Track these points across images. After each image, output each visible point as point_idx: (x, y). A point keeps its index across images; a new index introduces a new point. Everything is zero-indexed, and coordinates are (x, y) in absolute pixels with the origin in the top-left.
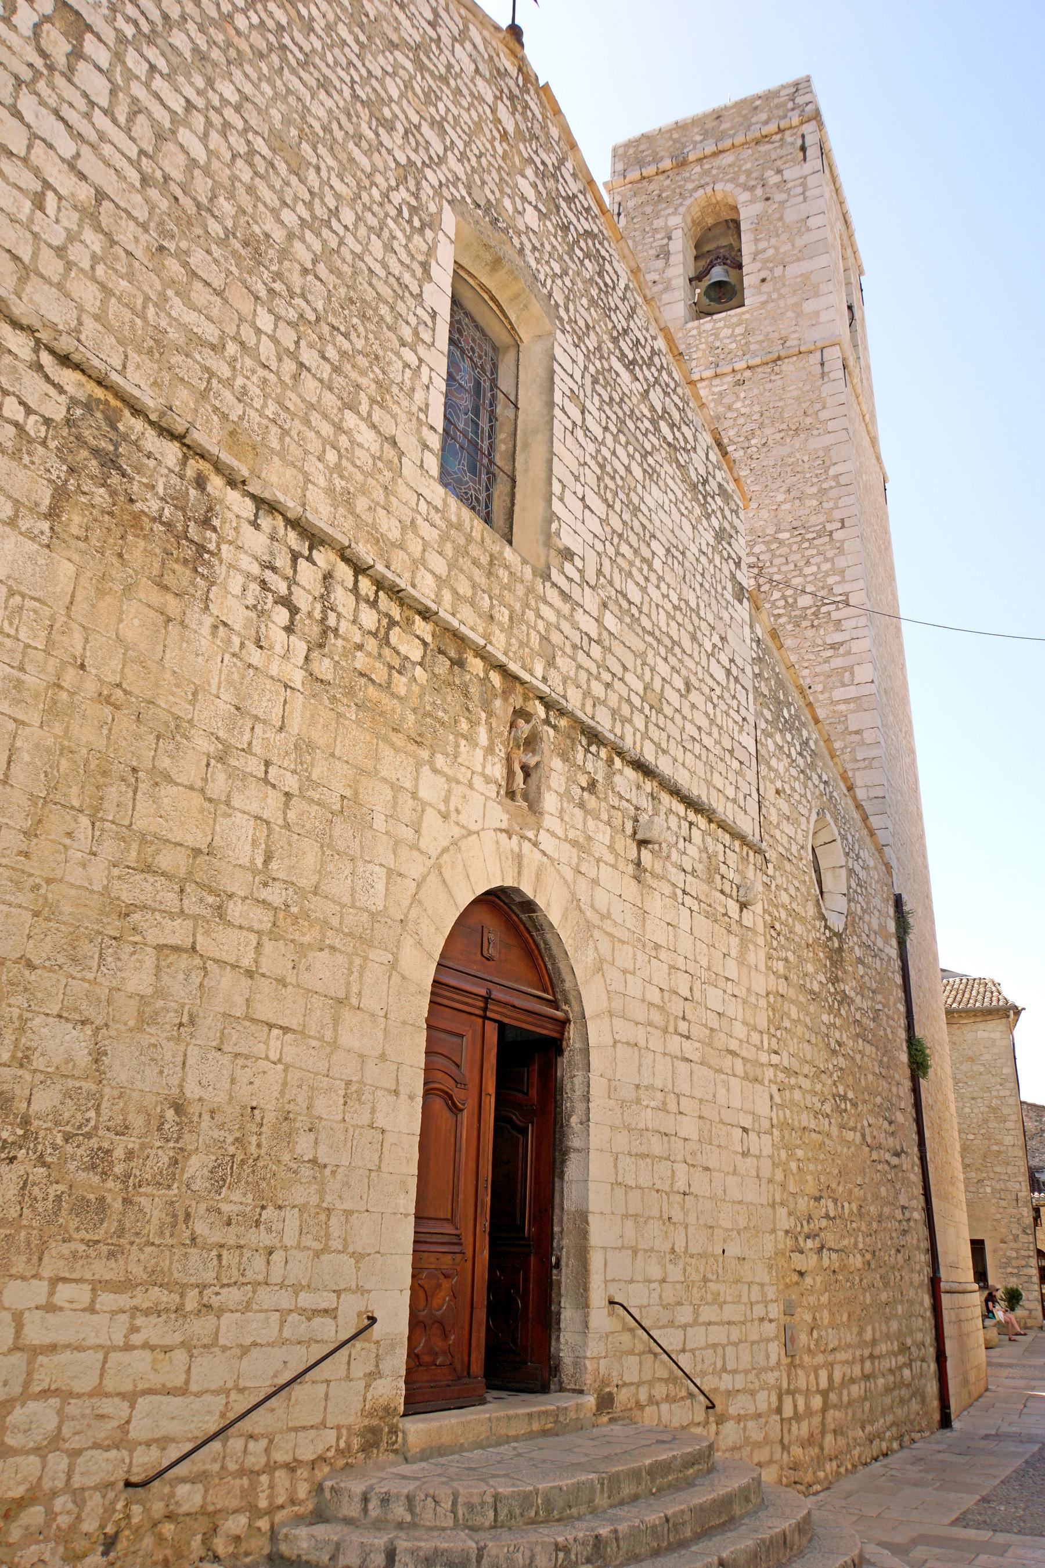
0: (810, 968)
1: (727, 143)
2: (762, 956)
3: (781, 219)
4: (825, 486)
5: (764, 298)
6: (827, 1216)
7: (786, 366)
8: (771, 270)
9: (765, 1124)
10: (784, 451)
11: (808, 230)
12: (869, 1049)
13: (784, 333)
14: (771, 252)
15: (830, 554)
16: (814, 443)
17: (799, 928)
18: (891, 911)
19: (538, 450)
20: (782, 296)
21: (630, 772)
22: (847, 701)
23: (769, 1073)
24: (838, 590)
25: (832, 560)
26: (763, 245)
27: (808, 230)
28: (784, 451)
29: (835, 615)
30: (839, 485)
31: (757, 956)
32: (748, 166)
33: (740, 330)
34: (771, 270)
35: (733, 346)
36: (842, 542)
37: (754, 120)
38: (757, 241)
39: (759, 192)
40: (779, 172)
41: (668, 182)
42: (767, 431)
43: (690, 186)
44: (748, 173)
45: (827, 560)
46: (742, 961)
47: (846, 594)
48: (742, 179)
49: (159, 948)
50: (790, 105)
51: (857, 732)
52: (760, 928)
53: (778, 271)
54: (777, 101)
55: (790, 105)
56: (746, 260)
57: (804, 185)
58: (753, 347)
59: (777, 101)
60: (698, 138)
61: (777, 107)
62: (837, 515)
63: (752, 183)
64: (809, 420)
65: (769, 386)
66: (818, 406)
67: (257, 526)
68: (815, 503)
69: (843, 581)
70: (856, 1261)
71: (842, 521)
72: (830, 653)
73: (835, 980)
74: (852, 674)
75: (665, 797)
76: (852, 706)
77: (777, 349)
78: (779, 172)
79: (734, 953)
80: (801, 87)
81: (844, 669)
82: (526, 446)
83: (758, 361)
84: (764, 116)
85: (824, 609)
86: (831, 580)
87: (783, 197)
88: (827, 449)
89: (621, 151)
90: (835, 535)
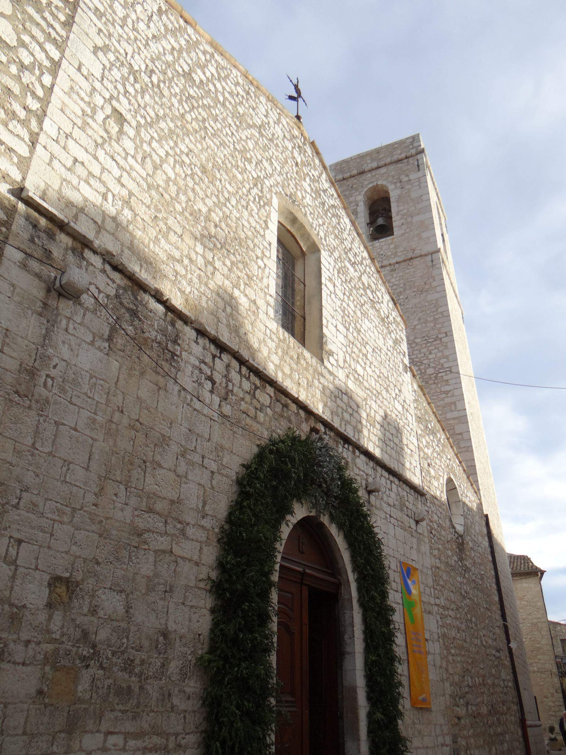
0: (449, 553)
1: (383, 163)
2: (428, 548)
3: (409, 196)
4: (437, 317)
5: (403, 232)
6: (468, 686)
7: (416, 262)
8: (406, 219)
9: (436, 636)
10: (416, 301)
11: (422, 201)
12: (480, 594)
14: (405, 211)
15: (441, 349)
16: (429, 298)
17: (443, 533)
18: (484, 523)
20: (411, 230)
21: (363, 457)
22: (454, 419)
23: (436, 608)
24: (446, 365)
25: (442, 352)
26: (401, 208)
27: (422, 201)
28: (416, 301)
29: (445, 378)
30: (443, 316)
31: (425, 548)
32: (393, 173)
33: (392, 246)
34: (406, 219)
35: (390, 253)
36: (447, 343)
37: (395, 153)
38: (398, 206)
39: (398, 185)
40: (407, 176)
41: (355, 181)
42: (408, 292)
43: (366, 183)
45: (439, 351)
46: (419, 551)
47: (450, 367)
48: (390, 179)
49: (156, 551)
50: (411, 147)
51: (459, 434)
52: (426, 534)
53: (409, 219)
54: (405, 145)
55: (411, 147)
58: (399, 254)
59: (405, 145)
60: (369, 161)
61: (406, 147)
62: (443, 330)
63: (395, 181)
64: (427, 287)
65: (407, 271)
66: (431, 280)
67: (197, 343)
68: (432, 325)
69: (448, 361)
70: (484, 710)
72: (444, 396)
73: (461, 559)
74: (455, 405)
75: (379, 469)
76: (456, 421)
77: (410, 255)
78: (407, 176)
79: (415, 547)
80: (415, 139)
81: (452, 403)
83: (401, 259)
84: (399, 152)
85: (440, 375)
88: (437, 300)
89: (333, 168)
90: (443, 340)
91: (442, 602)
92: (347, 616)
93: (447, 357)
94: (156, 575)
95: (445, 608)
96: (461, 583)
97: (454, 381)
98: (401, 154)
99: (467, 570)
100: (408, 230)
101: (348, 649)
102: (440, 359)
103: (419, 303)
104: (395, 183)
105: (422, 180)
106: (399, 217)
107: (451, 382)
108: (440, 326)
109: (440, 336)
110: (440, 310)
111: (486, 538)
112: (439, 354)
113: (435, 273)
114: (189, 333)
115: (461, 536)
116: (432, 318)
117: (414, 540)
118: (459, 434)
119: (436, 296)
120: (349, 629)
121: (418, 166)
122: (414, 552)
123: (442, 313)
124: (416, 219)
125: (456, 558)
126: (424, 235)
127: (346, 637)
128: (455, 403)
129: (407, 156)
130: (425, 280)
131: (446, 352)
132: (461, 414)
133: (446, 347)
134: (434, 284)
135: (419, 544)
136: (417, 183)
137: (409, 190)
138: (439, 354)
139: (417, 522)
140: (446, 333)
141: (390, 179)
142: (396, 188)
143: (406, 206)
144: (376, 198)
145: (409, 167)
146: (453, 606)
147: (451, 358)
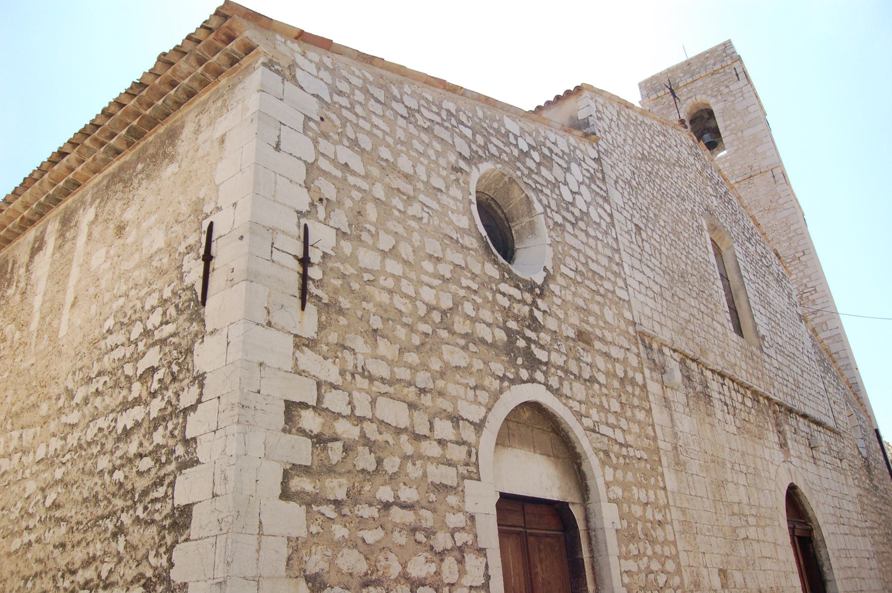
13: (750, 164)
14: (733, 125)
17: (856, 462)
19: (742, 297)
21: (801, 420)
24: (809, 285)
26: (728, 122)
29: (811, 298)
37: (708, 63)
38: (725, 121)
39: (719, 97)
44: (712, 89)
45: (800, 271)
47: (814, 287)
48: (709, 92)
51: (836, 353)
55: (724, 55)
56: (721, 131)
57: (741, 91)
60: (681, 75)
61: (718, 56)
62: (800, 249)
64: (774, 205)
65: (749, 190)
69: (811, 280)
71: (803, 251)
72: (813, 316)
73: (871, 480)
74: (826, 325)
76: (830, 341)
78: (727, 87)
81: (822, 323)
82: (737, 296)
83: (740, 179)
84: (712, 61)
85: (804, 295)
86: (805, 281)
87: (732, 99)
89: (643, 85)
91: (868, 524)
92: (822, 553)
93: (809, 276)
94: (747, 555)
95: (872, 528)
96: (876, 502)
97: (820, 301)
98: (714, 64)
99: (876, 488)
100: (741, 146)
101: (828, 578)
102: (802, 279)
103: (768, 223)
104: (716, 96)
105: (745, 90)
106: (727, 133)
107: (817, 302)
108: (795, 244)
109: (797, 255)
110: (792, 228)
111: (881, 453)
112: (801, 274)
113: (779, 189)
114: (709, 374)
115: (866, 459)
116: (785, 238)
117: (843, 476)
118: (836, 353)
119: (786, 213)
120: (826, 563)
121: (737, 75)
122: (845, 487)
123: (795, 231)
124: (747, 133)
125: (868, 481)
126: (760, 150)
127: (825, 569)
128: (826, 323)
129: (723, 63)
130: (770, 197)
131: (807, 272)
132: (835, 332)
133: (806, 266)
134: (781, 201)
135: (846, 478)
136: (740, 94)
137: (733, 101)
138: (801, 274)
139: (841, 460)
140: (803, 251)
141: (709, 92)
142: (717, 102)
143: (733, 120)
144: (695, 111)
145: (725, 78)
146: (876, 525)
147: (813, 277)
